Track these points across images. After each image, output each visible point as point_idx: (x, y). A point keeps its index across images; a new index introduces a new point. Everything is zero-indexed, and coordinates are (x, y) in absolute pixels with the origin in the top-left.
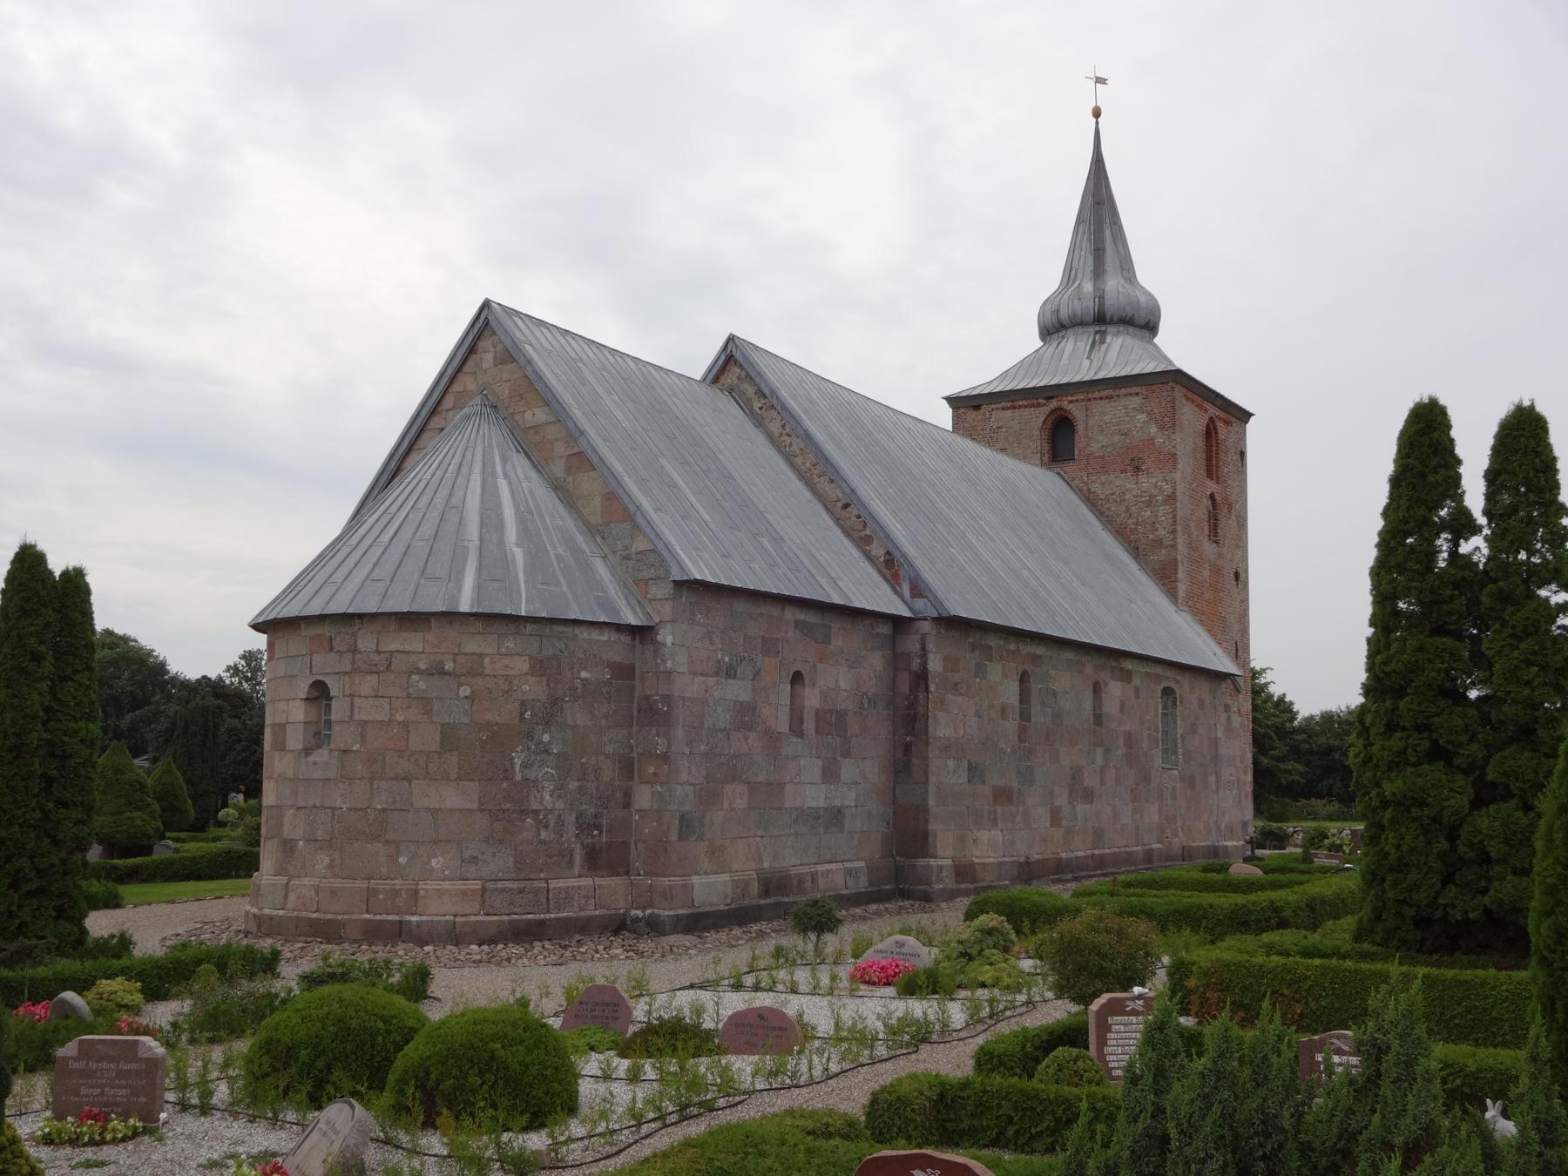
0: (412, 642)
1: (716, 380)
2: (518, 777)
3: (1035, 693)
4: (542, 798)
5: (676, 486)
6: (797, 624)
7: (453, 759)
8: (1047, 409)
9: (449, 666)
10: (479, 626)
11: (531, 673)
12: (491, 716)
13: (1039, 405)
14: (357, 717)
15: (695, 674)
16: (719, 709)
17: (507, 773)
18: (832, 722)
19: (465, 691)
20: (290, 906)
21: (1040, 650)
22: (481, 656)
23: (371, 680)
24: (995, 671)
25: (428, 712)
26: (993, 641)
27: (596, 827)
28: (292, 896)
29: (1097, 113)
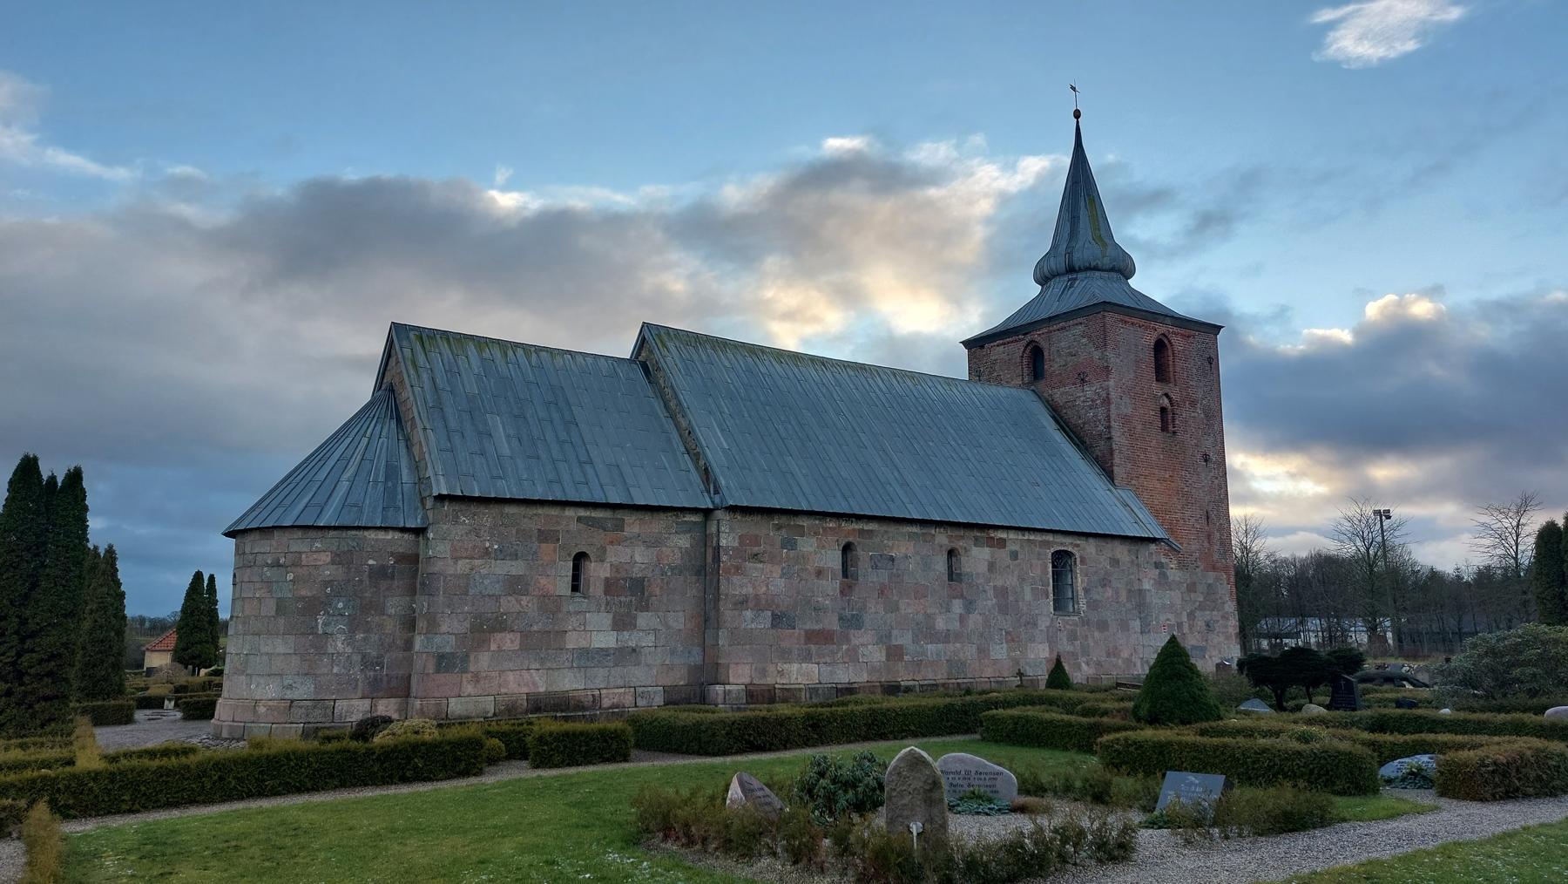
5: (722, 430)
6: (579, 519)
7: (282, 621)
8: (1024, 343)
10: (299, 533)
11: (333, 562)
12: (303, 593)
19: (290, 576)
24: (807, 545)
26: (805, 522)
29: (1077, 114)
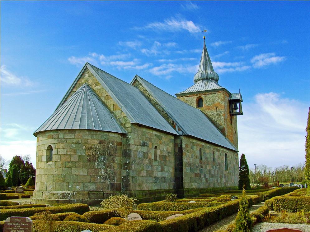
0: (72, 136)
1: (133, 84)
2: (96, 168)
3: (202, 153)
4: (102, 173)
6: (156, 135)
8: (197, 97)
9: (80, 142)
10: (87, 132)
13: (195, 96)
14: (59, 154)
15: (136, 145)
16: (140, 153)
17: (94, 167)
18: (163, 157)
20: (43, 197)
21: (203, 144)
22: (88, 139)
23: (62, 145)
25: (75, 152)
27: (114, 179)
28: (44, 195)
